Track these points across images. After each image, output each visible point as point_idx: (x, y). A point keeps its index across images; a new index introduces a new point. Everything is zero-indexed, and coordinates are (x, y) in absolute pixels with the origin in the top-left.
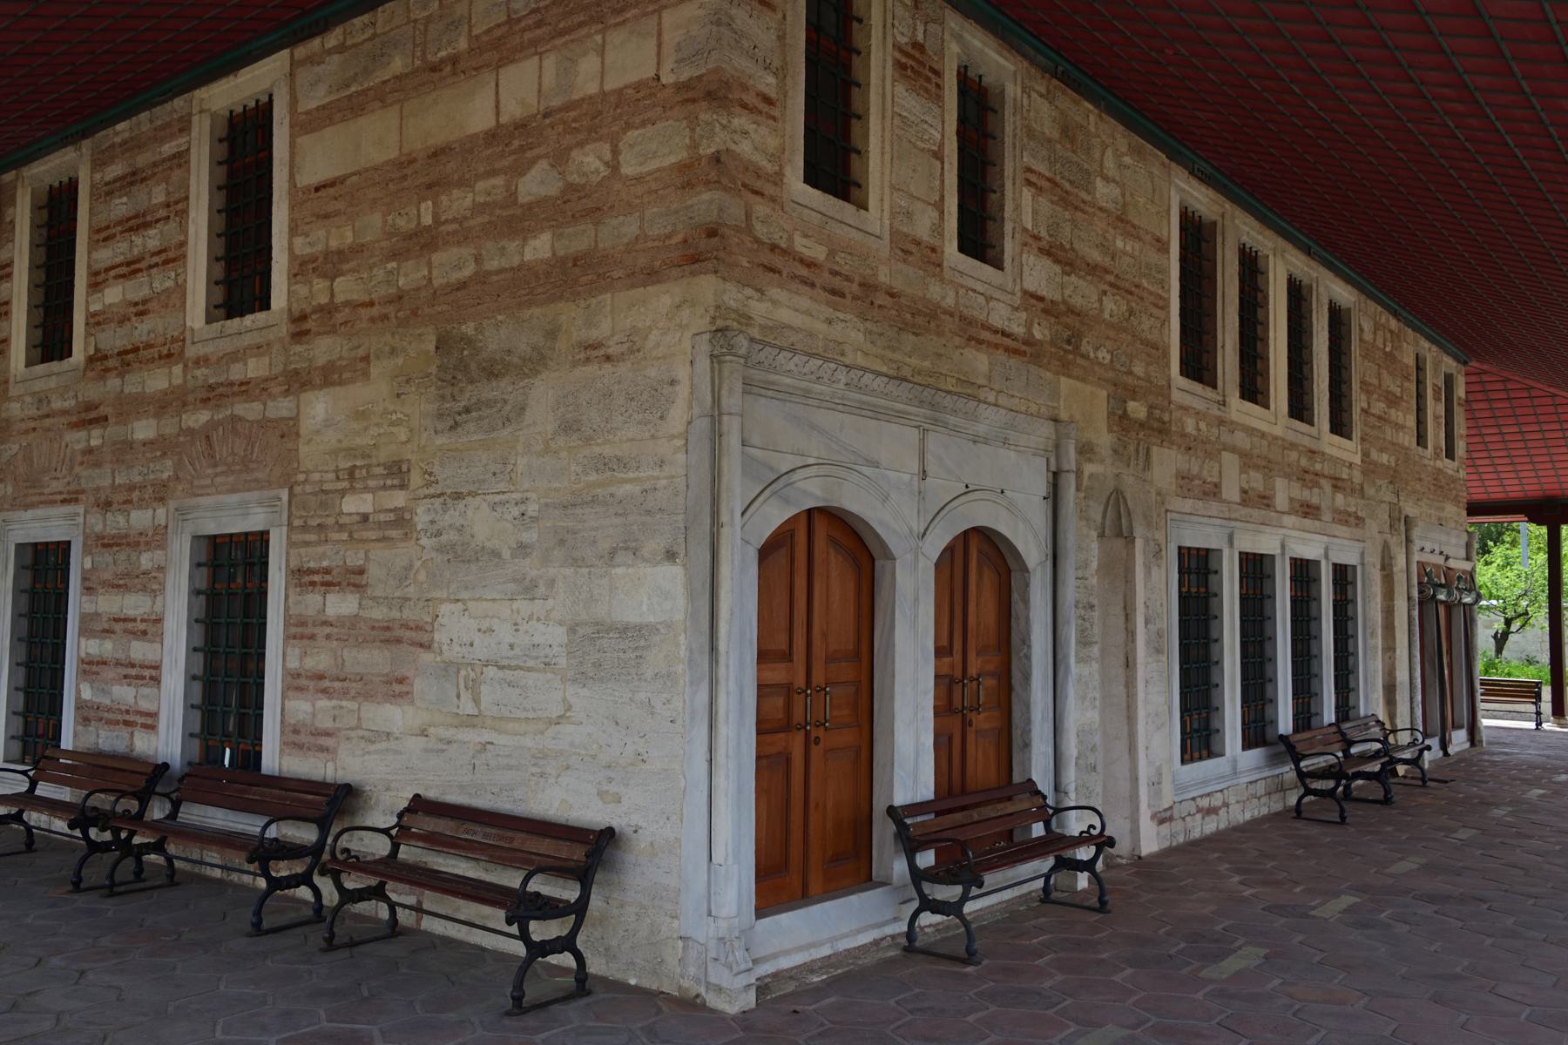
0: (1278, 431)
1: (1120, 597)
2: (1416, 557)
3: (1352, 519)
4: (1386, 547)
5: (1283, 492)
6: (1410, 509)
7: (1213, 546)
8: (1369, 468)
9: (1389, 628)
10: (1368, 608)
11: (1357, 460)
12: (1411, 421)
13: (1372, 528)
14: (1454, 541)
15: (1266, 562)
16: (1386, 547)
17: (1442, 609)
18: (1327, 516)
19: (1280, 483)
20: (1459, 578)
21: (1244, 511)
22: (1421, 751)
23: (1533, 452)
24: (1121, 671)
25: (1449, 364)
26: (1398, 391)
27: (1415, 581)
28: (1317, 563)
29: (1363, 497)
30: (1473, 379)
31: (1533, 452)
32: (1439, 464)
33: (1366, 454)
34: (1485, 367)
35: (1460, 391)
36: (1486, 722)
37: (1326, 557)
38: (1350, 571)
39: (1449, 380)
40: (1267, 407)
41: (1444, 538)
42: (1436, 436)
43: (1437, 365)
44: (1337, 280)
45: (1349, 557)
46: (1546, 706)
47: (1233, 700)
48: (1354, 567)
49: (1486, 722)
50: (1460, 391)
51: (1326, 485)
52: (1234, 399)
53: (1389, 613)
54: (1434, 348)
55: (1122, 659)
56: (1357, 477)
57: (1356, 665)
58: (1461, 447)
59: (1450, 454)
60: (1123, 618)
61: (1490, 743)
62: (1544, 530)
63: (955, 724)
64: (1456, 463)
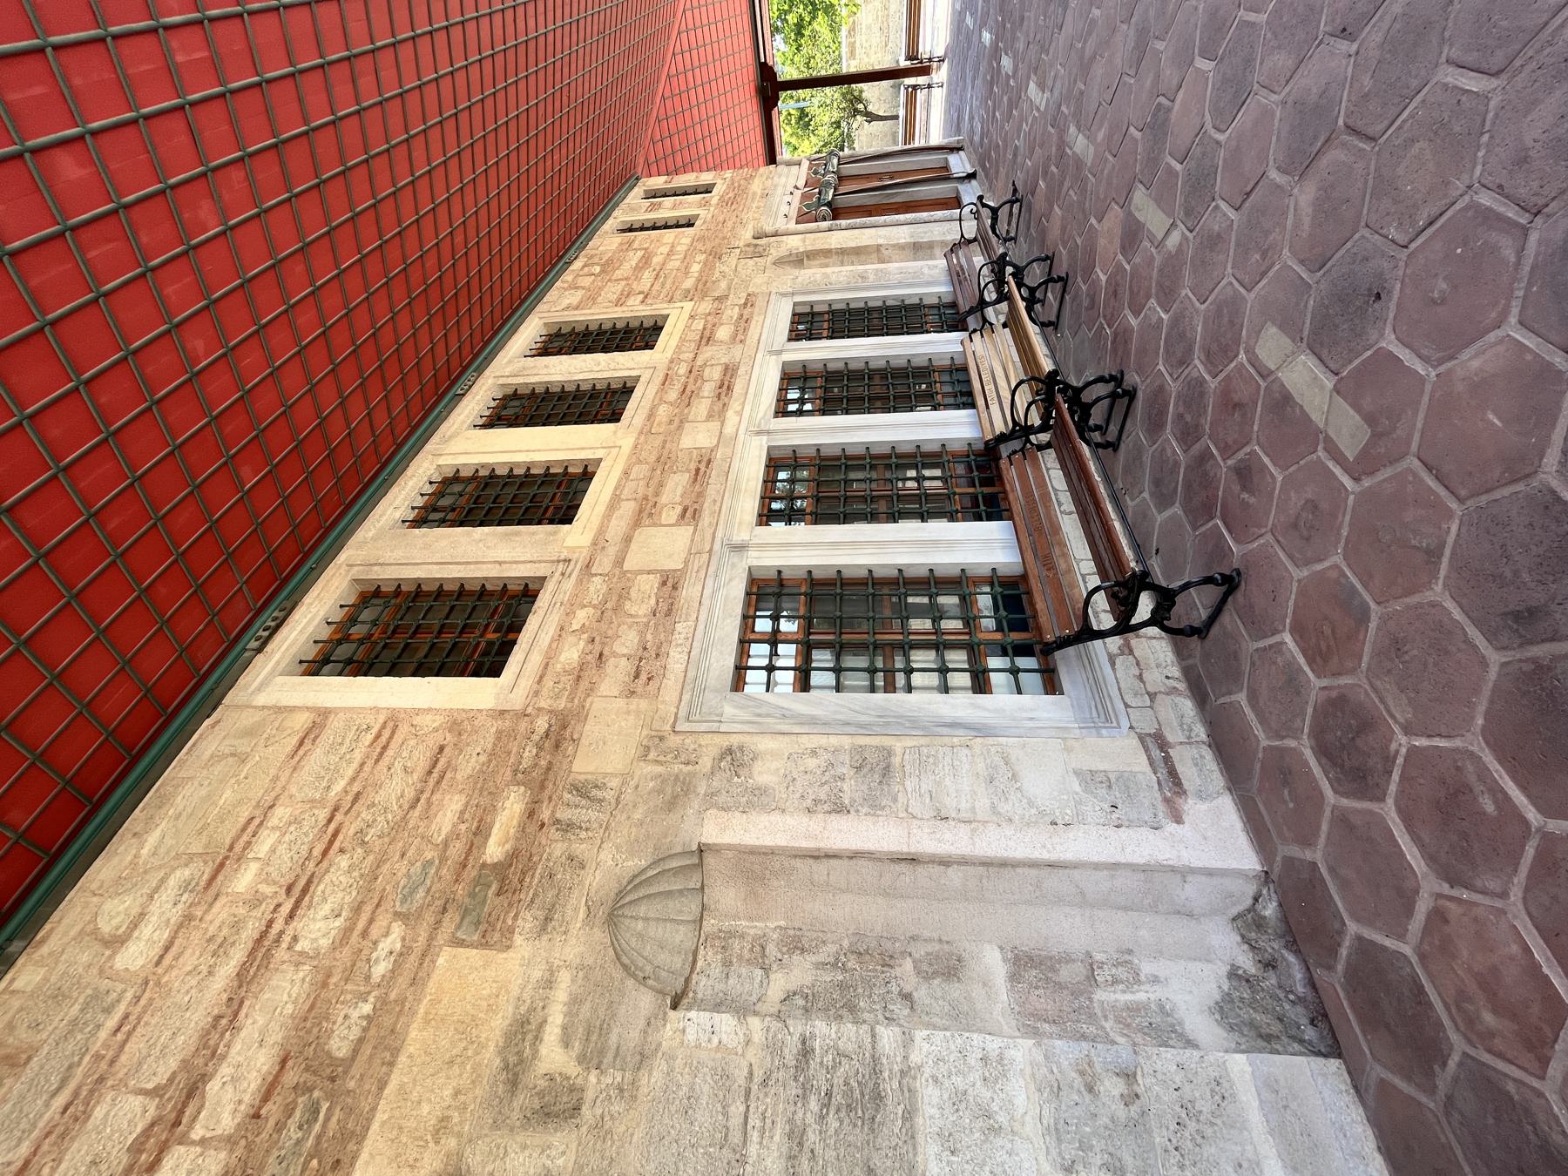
0: (627, 443)
1: (798, 863)
2: (792, 226)
3: (746, 312)
4: (779, 262)
5: (698, 436)
6: (747, 235)
7: (745, 575)
8: (701, 289)
9: (858, 253)
10: (838, 284)
11: (688, 306)
12: (669, 235)
13: (759, 282)
14: (783, 180)
15: (776, 454)
16: (779, 262)
17: (842, 190)
18: (737, 351)
19: (687, 441)
20: (816, 173)
21: (706, 519)
22: (984, 205)
23: (717, 110)
24: (920, 869)
25: (635, 197)
26: (640, 253)
27: (813, 225)
28: (795, 304)
29: (727, 297)
30: (654, 168)
31: (717, 110)
32: (714, 201)
33: (687, 295)
34: (642, 161)
35: (658, 182)
36: (38, 90)
37: (779, 352)
38: (800, 310)
39: (652, 195)
40: (600, 461)
41: (780, 191)
42: (690, 205)
43: (632, 209)
44: (507, 347)
45: (780, 318)
46: (921, 80)
47: (951, 544)
48: (795, 304)
49: (38, 90)
50: (658, 182)
51: (708, 352)
52: (575, 536)
53: (845, 254)
54: (615, 214)
55: (903, 867)
56: (706, 306)
57: (894, 297)
58: (706, 178)
59: (708, 190)
60: (833, 862)
61: (958, 131)
62: (783, 95)
63: (882, 506)
64: (719, 181)
